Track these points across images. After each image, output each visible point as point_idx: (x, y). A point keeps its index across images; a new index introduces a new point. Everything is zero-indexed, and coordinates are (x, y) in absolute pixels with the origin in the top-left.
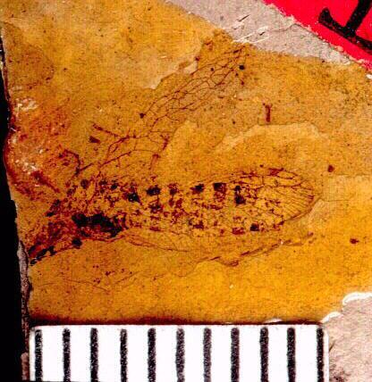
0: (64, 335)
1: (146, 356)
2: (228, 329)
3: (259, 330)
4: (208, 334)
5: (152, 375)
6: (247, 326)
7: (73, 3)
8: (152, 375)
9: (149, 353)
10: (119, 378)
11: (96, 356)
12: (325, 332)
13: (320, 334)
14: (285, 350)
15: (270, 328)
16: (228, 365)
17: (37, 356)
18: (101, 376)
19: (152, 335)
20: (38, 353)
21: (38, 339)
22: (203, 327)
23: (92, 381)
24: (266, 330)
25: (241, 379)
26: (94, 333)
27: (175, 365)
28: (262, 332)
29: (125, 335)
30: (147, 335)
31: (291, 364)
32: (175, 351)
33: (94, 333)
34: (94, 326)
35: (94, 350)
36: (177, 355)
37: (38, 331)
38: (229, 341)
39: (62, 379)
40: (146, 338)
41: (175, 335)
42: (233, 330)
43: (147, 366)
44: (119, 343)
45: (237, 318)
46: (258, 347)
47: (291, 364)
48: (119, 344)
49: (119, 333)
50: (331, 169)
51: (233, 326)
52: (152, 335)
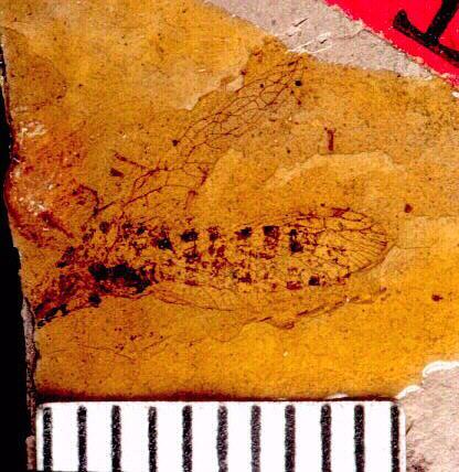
0: (79, 414)
1: (180, 440)
2: (281, 407)
3: (320, 408)
4: (256, 413)
5: (187, 464)
6: (305, 403)
7: (91, 4)
8: (187, 464)
9: (184, 436)
10: (146, 467)
11: (119, 440)
12: (401, 410)
13: (395, 413)
14: (352, 433)
15: (333, 405)
16: (282, 450)
17: (45, 440)
18: (124, 464)
19: (187, 414)
20: (47, 436)
21: (47, 418)
22: (250, 404)
23: (114, 470)
24: (329, 407)
25: (298, 468)
26: (116, 411)
27: (216, 451)
28: (323, 410)
29: (155, 413)
30: (181, 414)
31: (360, 450)
32: (216, 434)
33: (116, 411)
34: (116, 403)
35: (116, 432)
36: (219, 439)
37: (47, 409)
38: (283, 421)
39: (76, 469)
40: (180, 418)
41: (216, 414)
42: (287, 407)
43: (181, 452)
44: (147, 424)
45: (293, 393)
46: (318, 429)
47: (360, 450)
48: (147, 424)
49: (147, 411)
50: (408, 208)
51: (288, 403)
52: (187, 414)
